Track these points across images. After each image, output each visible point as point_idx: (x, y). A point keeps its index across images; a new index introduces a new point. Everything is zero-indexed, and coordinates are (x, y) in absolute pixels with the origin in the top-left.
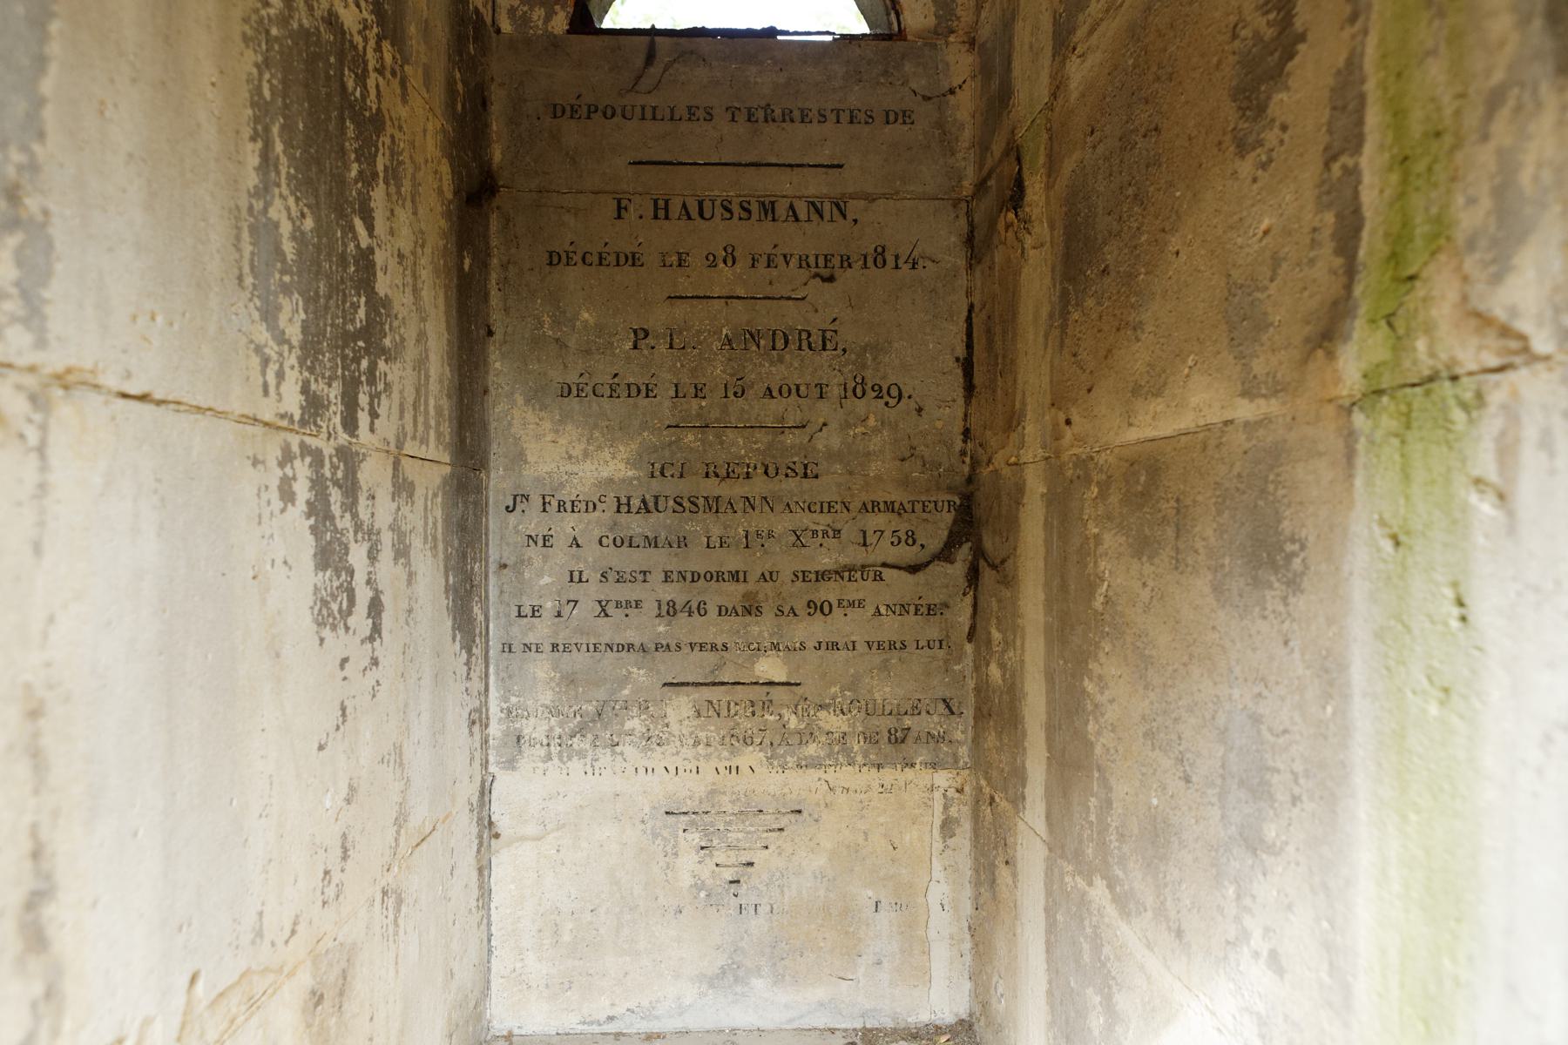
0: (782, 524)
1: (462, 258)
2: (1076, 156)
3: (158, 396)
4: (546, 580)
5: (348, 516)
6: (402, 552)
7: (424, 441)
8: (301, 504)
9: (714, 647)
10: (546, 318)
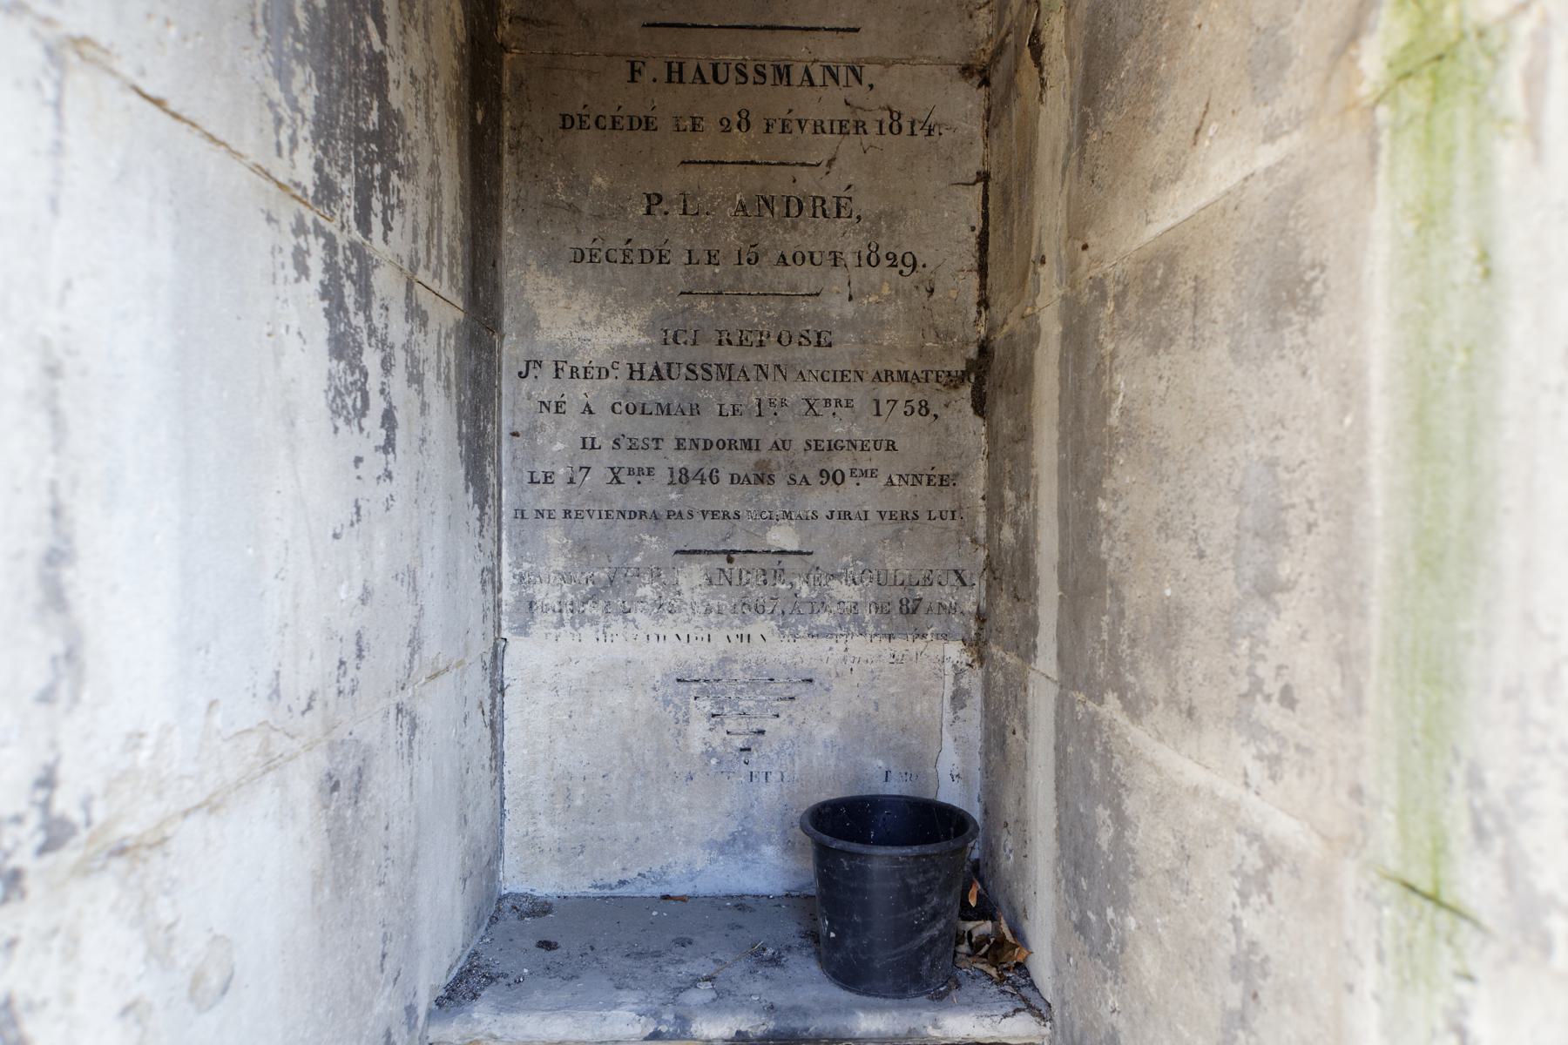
0: (795, 392)
4: (559, 446)
9: (726, 515)
10: (559, 183)
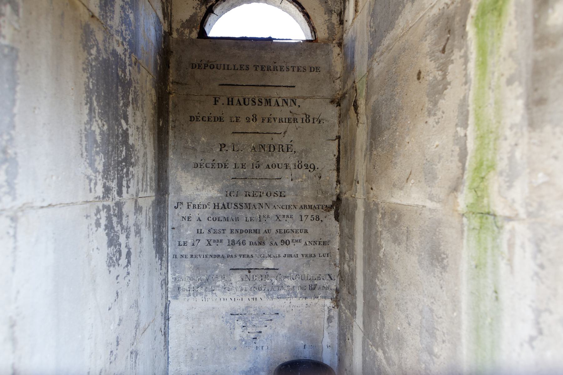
0: (272, 213)
1: (159, 122)
2: (375, 96)
3: (54, 204)
4: (189, 232)
5: (119, 225)
6: (138, 232)
7: (146, 191)
8: (103, 227)
9: (248, 256)
